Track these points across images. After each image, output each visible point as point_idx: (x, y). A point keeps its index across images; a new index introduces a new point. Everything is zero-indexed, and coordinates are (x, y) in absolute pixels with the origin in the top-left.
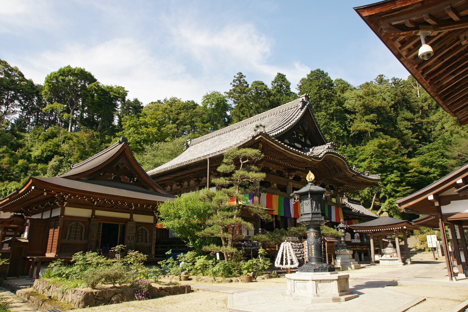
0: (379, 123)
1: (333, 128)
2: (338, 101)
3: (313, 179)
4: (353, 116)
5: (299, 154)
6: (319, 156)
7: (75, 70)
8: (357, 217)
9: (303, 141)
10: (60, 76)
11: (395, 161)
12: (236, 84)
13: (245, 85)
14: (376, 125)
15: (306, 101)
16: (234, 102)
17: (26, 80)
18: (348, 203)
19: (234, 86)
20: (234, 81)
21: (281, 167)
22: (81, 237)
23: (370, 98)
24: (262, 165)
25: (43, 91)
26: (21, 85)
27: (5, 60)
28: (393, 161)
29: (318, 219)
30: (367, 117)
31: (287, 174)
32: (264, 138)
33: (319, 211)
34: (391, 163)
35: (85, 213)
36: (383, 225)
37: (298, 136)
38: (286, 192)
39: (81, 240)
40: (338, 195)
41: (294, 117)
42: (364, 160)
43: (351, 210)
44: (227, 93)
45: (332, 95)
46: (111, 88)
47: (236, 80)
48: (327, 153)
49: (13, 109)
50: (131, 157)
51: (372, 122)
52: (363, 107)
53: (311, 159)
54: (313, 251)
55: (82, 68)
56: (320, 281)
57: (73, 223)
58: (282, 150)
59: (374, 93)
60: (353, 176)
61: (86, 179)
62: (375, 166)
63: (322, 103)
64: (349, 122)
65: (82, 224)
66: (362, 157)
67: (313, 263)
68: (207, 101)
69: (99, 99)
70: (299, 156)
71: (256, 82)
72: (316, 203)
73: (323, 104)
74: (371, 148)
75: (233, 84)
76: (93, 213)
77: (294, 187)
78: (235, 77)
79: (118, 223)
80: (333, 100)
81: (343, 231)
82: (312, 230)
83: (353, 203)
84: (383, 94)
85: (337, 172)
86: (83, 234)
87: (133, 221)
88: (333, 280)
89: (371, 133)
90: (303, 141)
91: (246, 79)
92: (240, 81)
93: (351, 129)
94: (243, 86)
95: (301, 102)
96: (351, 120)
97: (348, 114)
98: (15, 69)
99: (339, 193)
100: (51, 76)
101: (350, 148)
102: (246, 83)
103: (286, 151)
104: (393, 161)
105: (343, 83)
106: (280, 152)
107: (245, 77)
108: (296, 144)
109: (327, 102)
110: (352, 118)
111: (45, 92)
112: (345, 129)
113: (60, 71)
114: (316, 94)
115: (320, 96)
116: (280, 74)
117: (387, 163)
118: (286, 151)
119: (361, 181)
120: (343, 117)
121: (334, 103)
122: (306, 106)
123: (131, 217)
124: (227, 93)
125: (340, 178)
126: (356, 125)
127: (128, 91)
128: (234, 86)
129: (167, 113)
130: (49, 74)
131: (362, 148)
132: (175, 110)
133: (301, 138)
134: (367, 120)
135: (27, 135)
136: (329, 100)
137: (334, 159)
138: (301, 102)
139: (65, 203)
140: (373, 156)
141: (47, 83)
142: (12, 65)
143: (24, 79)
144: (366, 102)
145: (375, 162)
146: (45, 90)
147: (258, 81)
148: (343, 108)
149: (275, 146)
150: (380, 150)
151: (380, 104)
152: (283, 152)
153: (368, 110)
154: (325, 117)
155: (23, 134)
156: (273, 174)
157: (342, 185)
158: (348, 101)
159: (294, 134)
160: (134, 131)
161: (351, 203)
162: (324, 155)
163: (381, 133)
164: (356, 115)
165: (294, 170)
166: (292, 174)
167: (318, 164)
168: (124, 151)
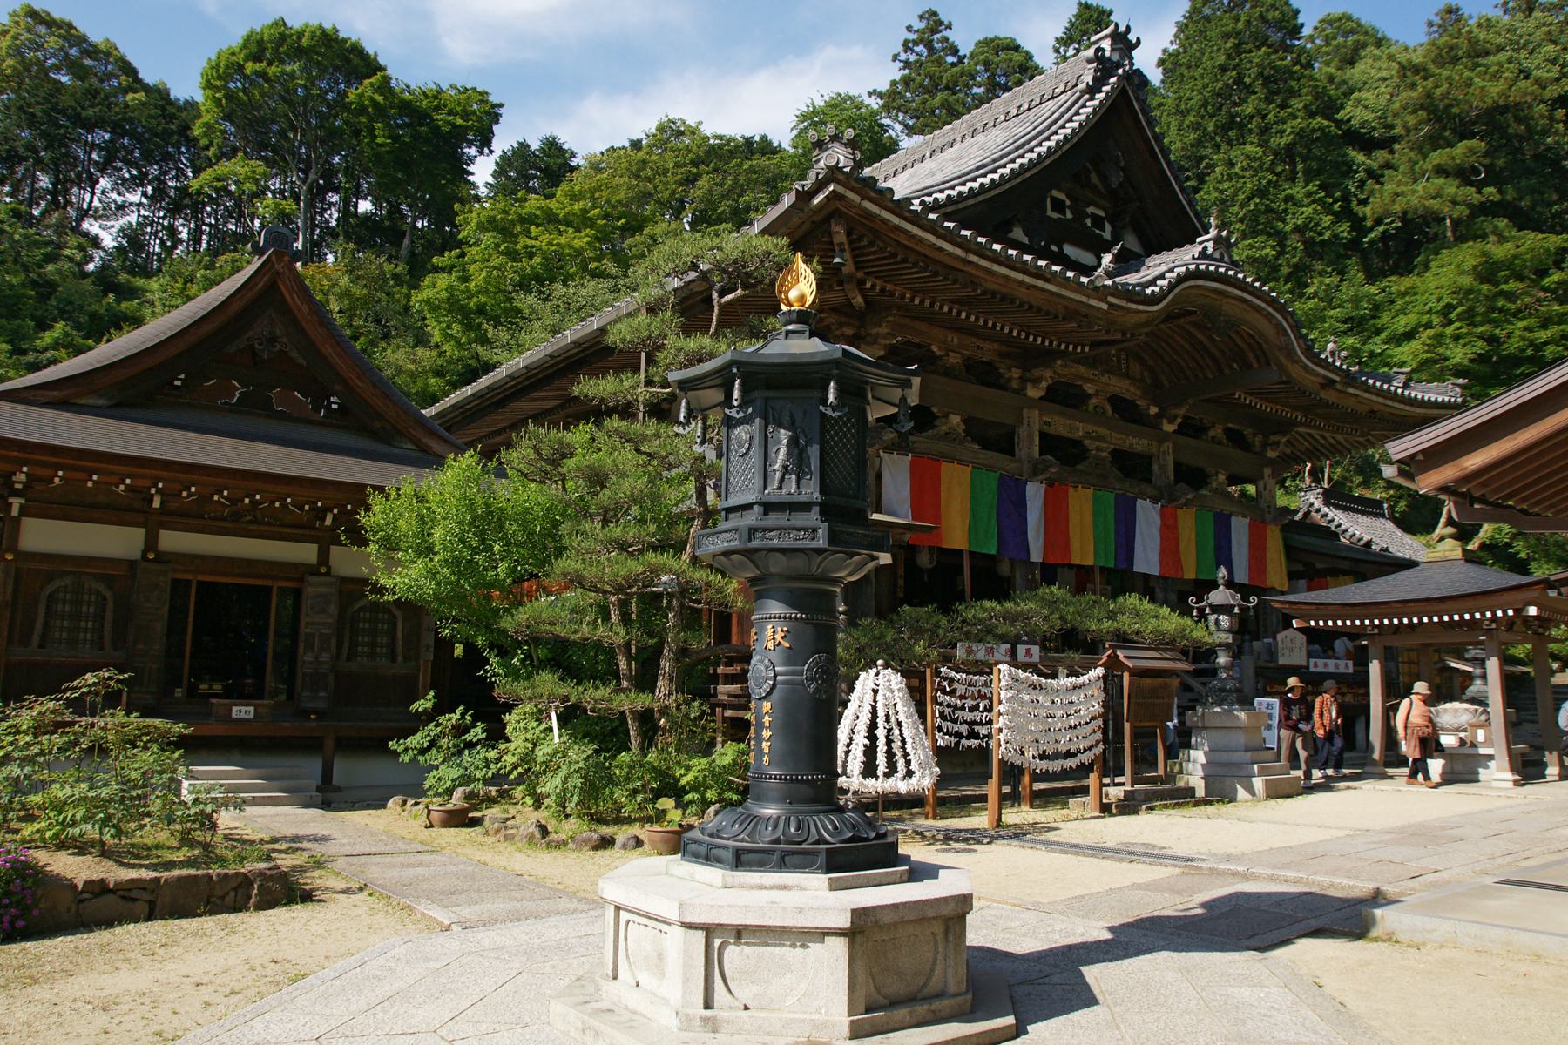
0: (1494, 177)
2: (1317, 97)
3: (810, 299)
4: (1381, 155)
5: (1039, 274)
7: (300, 35)
8: (1345, 565)
10: (246, 60)
11: (1549, 333)
12: (913, 58)
13: (950, 59)
14: (1480, 185)
15: (1116, 57)
16: (906, 126)
17: (146, 88)
18: (1326, 510)
19: (907, 64)
20: (907, 46)
21: (987, 345)
22: (101, 637)
23: (1461, 72)
24: (883, 330)
25: (199, 122)
26: (127, 106)
27: (67, 18)
28: (1543, 335)
30: (1438, 157)
31: (1016, 373)
32: (850, 194)
34: (1532, 343)
35: (117, 541)
36: (1428, 600)
37: (1080, 215)
38: (1011, 453)
39: (102, 649)
40: (1267, 471)
41: (1053, 129)
42: (1409, 336)
43: (1335, 536)
44: (880, 95)
45: (1292, 74)
46: (435, 97)
47: (916, 43)
48: (1189, 276)
49: (119, 199)
50: (305, 308)
51: (1464, 174)
52: (1422, 114)
53: (1103, 300)
54: (766, 734)
55: (328, 26)
56: (740, 933)
57: (58, 583)
58: (950, 254)
59: (1478, 52)
60: (1323, 386)
61: (101, 402)
62: (1459, 355)
64: (1362, 183)
65: (101, 587)
66: (1403, 323)
67: (770, 811)
69: (396, 138)
70: (1040, 283)
71: (986, 42)
72: (793, 443)
73: (1250, 110)
74: (1444, 281)
75: (903, 57)
76: (151, 543)
77: (1051, 430)
78: (909, 29)
79: (189, 577)
80: (1294, 93)
81: (1225, 620)
82: (776, 608)
83: (1345, 509)
84: (1523, 54)
85: (1249, 367)
86: (108, 627)
87: (328, 574)
88: (823, 934)
89: (1456, 223)
91: (952, 36)
92: (929, 45)
93: (1368, 210)
94: (940, 61)
95: (1089, 61)
96: (1371, 173)
97: (1361, 149)
98: (102, 47)
100: (218, 65)
101: (1356, 287)
102: (954, 51)
103: (973, 258)
104: (1543, 335)
105: (1352, 32)
106: (948, 269)
107: (949, 27)
108: (1069, 250)
109: (1269, 101)
110: (1375, 165)
111: (206, 124)
112: (1346, 214)
113: (248, 40)
114: (1224, 69)
115: (1239, 80)
116: (1087, 7)
117: (1514, 345)
118: (973, 258)
119: (1363, 409)
120: (1337, 163)
121: (1297, 104)
122: (1113, 80)
123: (324, 557)
124: (880, 95)
125: (1259, 393)
126: (1389, 188)
127: (501, 106)
128: (907, 64)
129: (650, 180)
130: (214, 58)
131: (1407, 282)
132: (676, 165)
133: (1098, 223)
134: (1441, 171)
135: (154, 284)
136: (1277, 93)
137: (1229, 308)
138: (1089, 61)
139: (16, 503)
140: (1453, 316)
141: (209, 92)
142: (96, 37)
143: (137, 83)
144: (1438, 92)
145: (1456, 338)
146: (205, 120)
147: (997, 38)
148: (1338, 123)
149: (913, 236)
150: (1485, 288)
151: (1500, 94)
152: (960, 266)
153: (1446, 122)
155: (140, 282)
156: (948, 372)
157: (1284, 427)
158: (1364, 95)
160: (497, 246)
161: (1337, 507)
162: (1171, 287)
163: (1502, 223)
164: (1392, 152)
165: (1046, 356)
166: (1036, 373)
167: (1146, 324)
168: (273, 286)
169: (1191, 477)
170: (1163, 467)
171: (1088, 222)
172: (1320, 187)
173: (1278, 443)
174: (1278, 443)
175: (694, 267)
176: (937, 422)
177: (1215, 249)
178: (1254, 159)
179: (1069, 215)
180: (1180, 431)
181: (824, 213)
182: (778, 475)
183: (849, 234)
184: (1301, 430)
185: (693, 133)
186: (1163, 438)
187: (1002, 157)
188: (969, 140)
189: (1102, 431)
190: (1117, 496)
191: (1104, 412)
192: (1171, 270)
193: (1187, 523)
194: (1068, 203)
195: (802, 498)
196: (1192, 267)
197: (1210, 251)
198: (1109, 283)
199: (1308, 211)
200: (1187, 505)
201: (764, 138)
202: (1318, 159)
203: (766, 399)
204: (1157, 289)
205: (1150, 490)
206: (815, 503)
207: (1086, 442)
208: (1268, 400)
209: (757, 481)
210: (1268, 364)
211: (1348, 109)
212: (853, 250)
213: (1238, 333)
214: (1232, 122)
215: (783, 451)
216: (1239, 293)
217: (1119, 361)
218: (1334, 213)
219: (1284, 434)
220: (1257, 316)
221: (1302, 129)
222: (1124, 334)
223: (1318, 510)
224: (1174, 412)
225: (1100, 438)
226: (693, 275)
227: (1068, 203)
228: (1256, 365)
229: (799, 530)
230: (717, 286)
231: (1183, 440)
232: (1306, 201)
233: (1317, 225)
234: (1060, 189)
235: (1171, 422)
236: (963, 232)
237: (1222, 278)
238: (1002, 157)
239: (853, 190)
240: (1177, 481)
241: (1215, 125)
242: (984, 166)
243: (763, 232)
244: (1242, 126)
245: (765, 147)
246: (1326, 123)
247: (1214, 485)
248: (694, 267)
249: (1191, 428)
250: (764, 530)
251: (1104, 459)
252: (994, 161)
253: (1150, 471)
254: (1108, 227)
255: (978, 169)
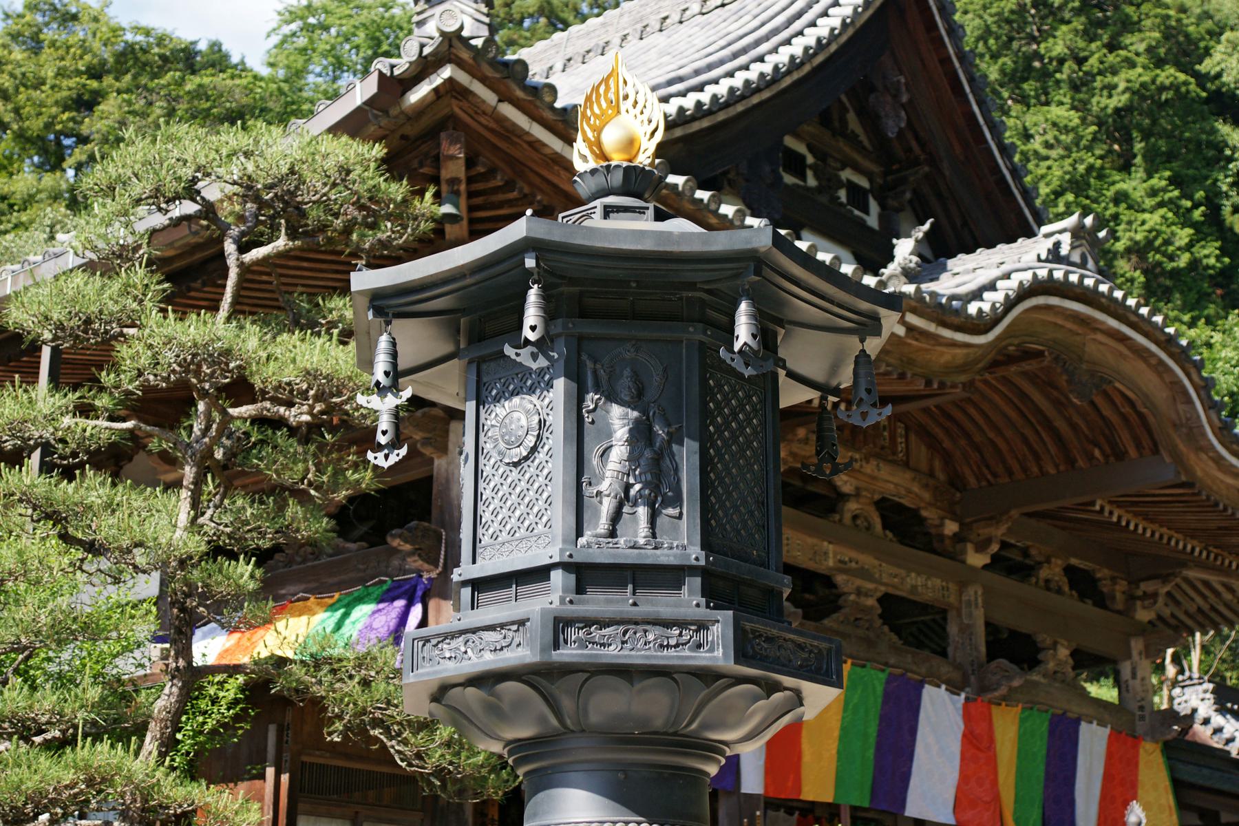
1: (1126, 215)
2: (1169, 34)
6: (973, 308)
9: (873, 221)
18: (1218, 720)
29: (642, 649)
33: (682, 541)
37: (829, 183)
40: (1137, 645)
41: (797, 25)
48: (1038, 288)
63: (1057, 46)
68: (302, 41)
72: (640, 435)
73: (1059, 49)
80: (1130, 26)
85: (1120, 455)
90: (873, 221)
99: (1143, 630)
121: (1137, 43)
132: (61, 73)
136: (1102, 24)
137: (1097, 349)
148: (1201, 79)
154: (1067, 139)
157: (1164, 565)
159: (796, 164)
162: (1010, 304)
167: (963, 368)
169: (1014, 648)
170: (966, 630)
171: (842, 195)
172: (1173, 181)
173: (1155, 595)
174: (1155, 595)
175: (191, 192)
176: (1040, 656)
177: (1073, 247)
178: (1067, 130)
179: (812, 182)
180: (997, 563)
181: (426, 122)
182: (607, 507)
183: (470, 163)
184: (1192, 574)
185: (96, 20)
186: (966, 578)
187: (710, 67)
188: (633, 43)
189: (867, 560)
190: (891, 679)
191: (869, 528)
192: (1007, 276)
193: (1007, 727)
194: (810, 159)
195: (665, 557)
196: (1043, 273)
197: (1064, 250)
198: (910, 289)
199: (1153, 219)
200: (1007, 699)
201: (216, 46)
202: (1169, 136)
203: (581, 339)
204: (986, 307)
205: (945, 669)
206: (691, 570)
207: (840, 579)
208: (1146, 517)
209: (559, 516)
210: (1155, 450)
211: (1217, 57)
212: (471, 195)
213: (1106, 394)
214: (1029, 68)
215: (619, 452)
216: (1113, 323)
217: (893, 438)
218: (1194, 225)
219: (1165, 579)
220: (1141, 365)
221: (1143, 85)
222: (928, 383)
223: (1206, 722)
224: (985, 532)
225: (864, 573)
226: (189, 208)
227: (810, 159)
228: (1133, 453)
229: (667, 624)
230: (235, 231)
231: (996, 579)
232: (1149, 203)
233: (1167, 242)
234: (798, 136)
235: (981, 547)
236: (672, 179)
237: (1088, 297)
238: (710, 67)
239: (484, 80)
240: (991, 656)
241: (1002, 71)
242: (680, 79)
243: (335, 130)
244: (1045, 75)
245: (218, 60)
246: (1182, 77)
247: (1051, 665)
248: (191, 192)
249: (1012, 564)
250: (588, 622)
251: (867, 610)
252: (697, 72)
253: (943, 634)
254: (874, 206)
255: (670, 83)
